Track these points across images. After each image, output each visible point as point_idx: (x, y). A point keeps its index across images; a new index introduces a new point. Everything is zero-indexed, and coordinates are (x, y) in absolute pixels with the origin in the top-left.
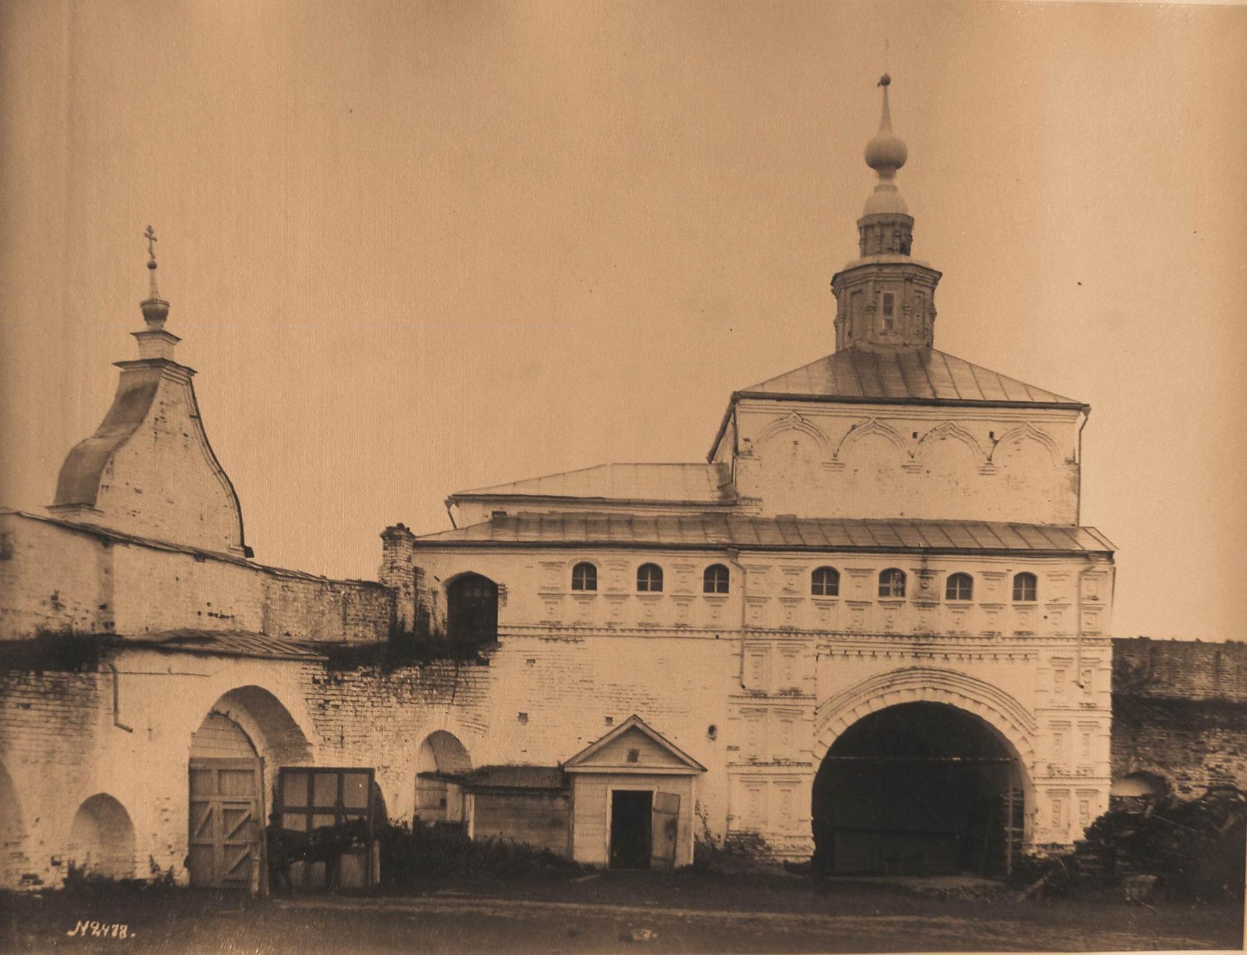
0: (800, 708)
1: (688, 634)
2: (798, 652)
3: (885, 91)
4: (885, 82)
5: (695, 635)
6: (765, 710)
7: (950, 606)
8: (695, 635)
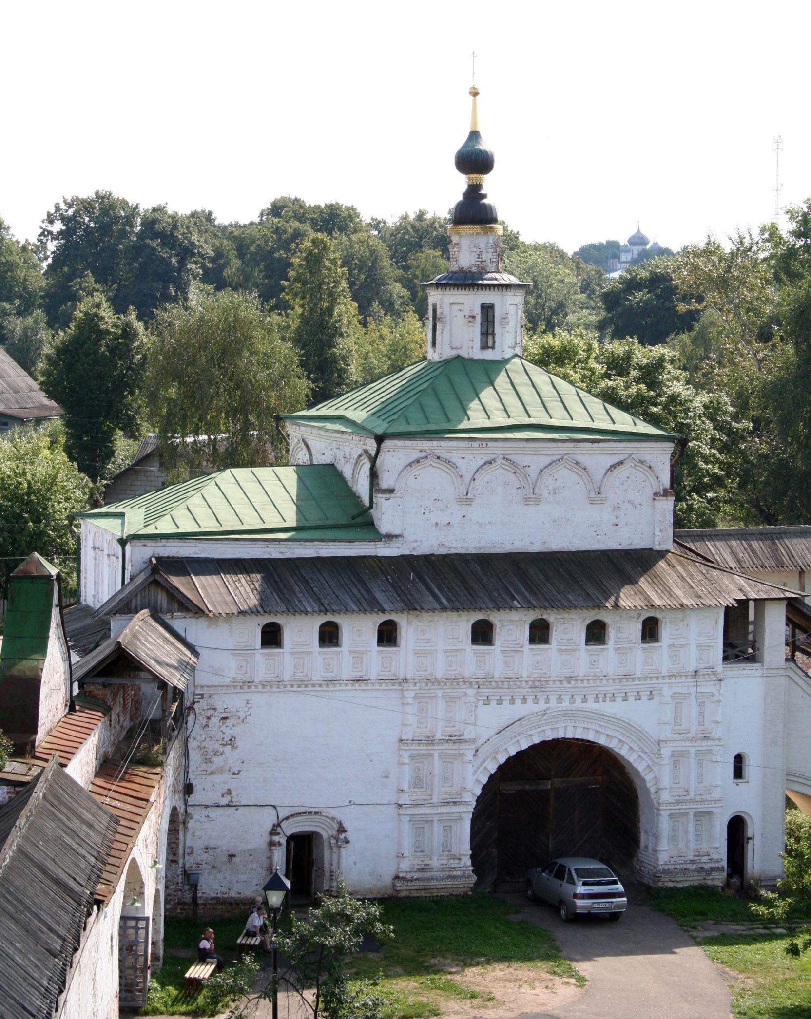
0: (462, 752)
3: (474, 103)
4: (475, 94)
6: (431, 755)
7: (531, 650)
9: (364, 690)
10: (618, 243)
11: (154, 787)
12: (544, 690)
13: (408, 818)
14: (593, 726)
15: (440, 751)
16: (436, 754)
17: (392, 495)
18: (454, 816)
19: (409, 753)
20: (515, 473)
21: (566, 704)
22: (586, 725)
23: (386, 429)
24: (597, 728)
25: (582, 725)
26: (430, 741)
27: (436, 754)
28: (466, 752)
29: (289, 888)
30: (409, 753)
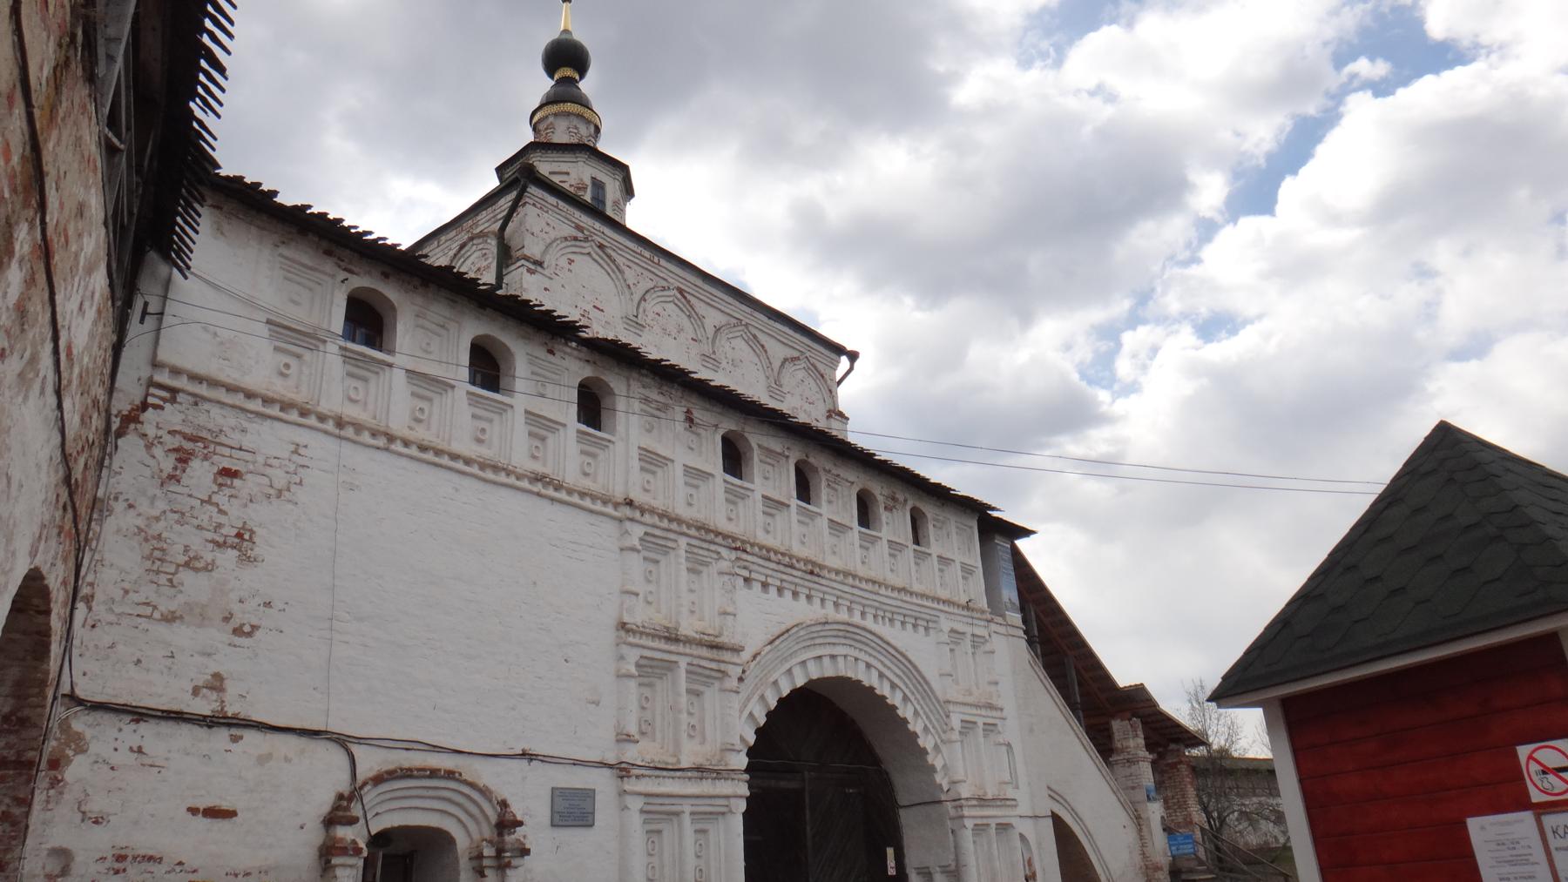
0: (723, 667)
1: (550, 492)
2: (707, 564)
5: (563, 495)
6: (671, 666)
8: (563, 495)
12: (816, 579)
16: (683, 663)
17: (539, 269)
20: (689, 317)
26: (672, 637)
27: (683, 663)
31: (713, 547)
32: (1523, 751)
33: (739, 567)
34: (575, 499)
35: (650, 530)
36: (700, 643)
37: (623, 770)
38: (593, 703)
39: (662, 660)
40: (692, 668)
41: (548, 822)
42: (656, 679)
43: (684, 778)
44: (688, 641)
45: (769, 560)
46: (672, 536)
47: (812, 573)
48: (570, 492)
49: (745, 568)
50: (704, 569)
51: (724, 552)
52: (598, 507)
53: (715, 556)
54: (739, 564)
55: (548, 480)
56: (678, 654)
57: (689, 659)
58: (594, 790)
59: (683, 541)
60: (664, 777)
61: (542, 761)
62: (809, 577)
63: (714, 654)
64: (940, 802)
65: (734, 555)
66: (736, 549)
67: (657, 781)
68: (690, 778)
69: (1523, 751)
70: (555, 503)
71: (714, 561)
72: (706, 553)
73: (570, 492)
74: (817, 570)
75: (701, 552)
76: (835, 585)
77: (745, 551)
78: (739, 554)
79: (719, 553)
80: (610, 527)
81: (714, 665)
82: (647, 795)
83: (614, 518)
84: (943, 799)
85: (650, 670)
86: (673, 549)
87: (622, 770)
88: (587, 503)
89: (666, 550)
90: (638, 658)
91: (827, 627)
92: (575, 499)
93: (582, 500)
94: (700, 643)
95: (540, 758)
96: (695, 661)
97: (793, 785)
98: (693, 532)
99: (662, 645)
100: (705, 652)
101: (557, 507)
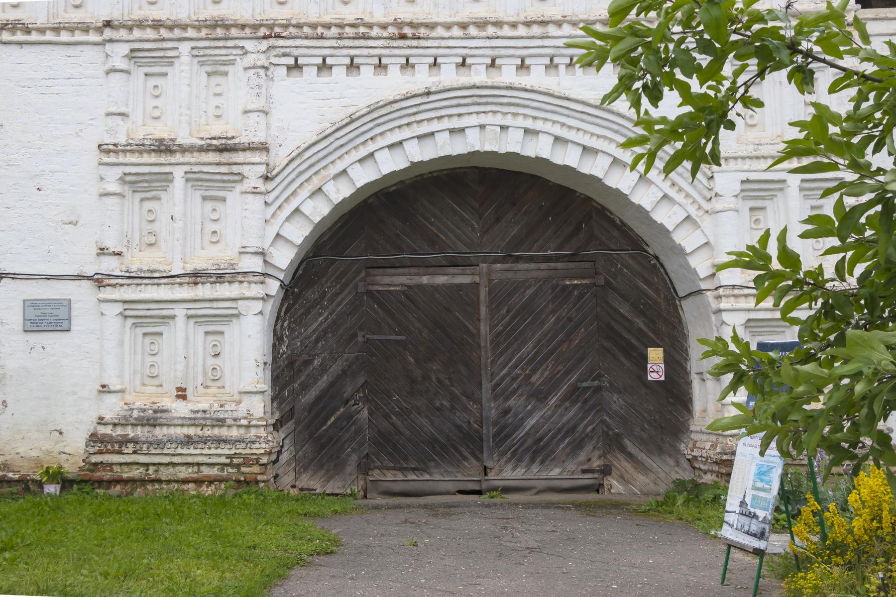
0: (235, 169)
1: (20, 37)
2: (232, 63)
5: (34, 37)
6: (167, 178)
8: (34, 37)
9: (20, 44)
10: (840, 115)
11: (173, 317)
12: (423, 43)
13: (119, 308)
14: (548, 127)
15: (187, 168)
16: (178, 173)
18: (222, 308)
19: (119, 171)
21: (479, 75)
22: (529, 124)
23: (688, 171)
24: (558, 131)
25: (520, 122)
26: (163, 147)
27: (178, 173)
28: (245, 170)
29: (765, 432)
30: (119, 171)
31: (230, 43)
32: (663, 378)
33: (276, 56)
34: (49, 36)
35: (194, 44)
36: (202, 149)
37: (99, 281)
38: (71, 223)
39: (150, 174)
40: (189, 176)
41: (20, 328)
42: (161, 192)
43: (173, 284)
44: (185, 149)
45: (322, 37)
46: (170, 45)
47: (403, 37)
48: (42, 31)
49: (285, 55)
50: (230, 69)
51: (249, 45)
52: (79, 37)
53: (239, 52)
54: (275, 53)
55: (10, 26)
56: (170, 164)
57: (187, 168)
58: (70, 300)
59: (185, 48)
60: (146, 285)
61: (13, 278)
62: (400, 43)
63: (226, 157)
64: (700, 292)
65: (264, 45)
66: (265, 37)
67: (139, 288)
68: (181, 284)
69: (663, 378)
70: (24, 46)
71: (238, 58)
72: (224, 52)
73: (42, 31)
74: (408, 31)
75: (217, 52)
76: (299, 42)
77: (279, 36)
78: (273, 42)
79: (243, 48)
80: (92, 54)
81: (223, 169)
82: (125, 302)
83: (95, 44)
84: (703, 288)
85: (146, 185)
86: (178, 57)
87: (97, 280)
88: (65, 37)
89: (170, 61)
90: (183, 174)
91: (432, 98)
92: (49, 36)
93: (73, 36)
94: (202, 149)
95: (10, 276)
96: (196, 169)
97: (465, 280)
98: (191, 33)
99: (153, 158)
100: (212, 157)
101: (27, 49)
